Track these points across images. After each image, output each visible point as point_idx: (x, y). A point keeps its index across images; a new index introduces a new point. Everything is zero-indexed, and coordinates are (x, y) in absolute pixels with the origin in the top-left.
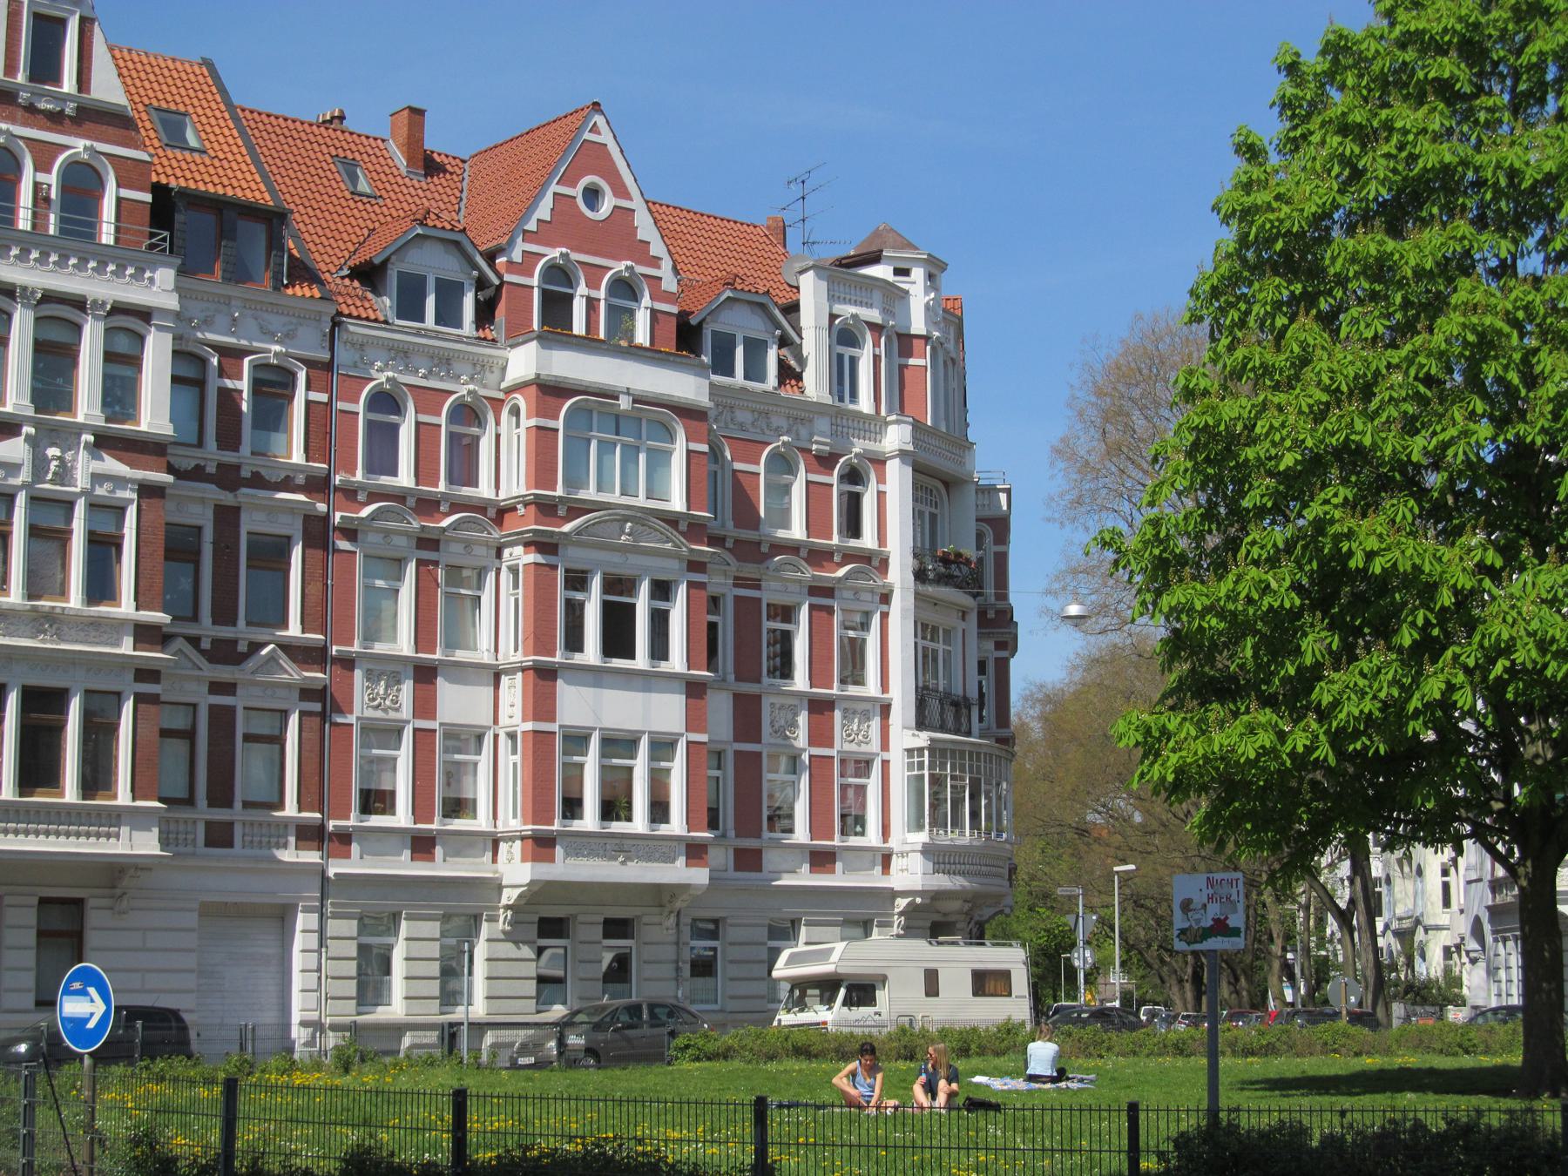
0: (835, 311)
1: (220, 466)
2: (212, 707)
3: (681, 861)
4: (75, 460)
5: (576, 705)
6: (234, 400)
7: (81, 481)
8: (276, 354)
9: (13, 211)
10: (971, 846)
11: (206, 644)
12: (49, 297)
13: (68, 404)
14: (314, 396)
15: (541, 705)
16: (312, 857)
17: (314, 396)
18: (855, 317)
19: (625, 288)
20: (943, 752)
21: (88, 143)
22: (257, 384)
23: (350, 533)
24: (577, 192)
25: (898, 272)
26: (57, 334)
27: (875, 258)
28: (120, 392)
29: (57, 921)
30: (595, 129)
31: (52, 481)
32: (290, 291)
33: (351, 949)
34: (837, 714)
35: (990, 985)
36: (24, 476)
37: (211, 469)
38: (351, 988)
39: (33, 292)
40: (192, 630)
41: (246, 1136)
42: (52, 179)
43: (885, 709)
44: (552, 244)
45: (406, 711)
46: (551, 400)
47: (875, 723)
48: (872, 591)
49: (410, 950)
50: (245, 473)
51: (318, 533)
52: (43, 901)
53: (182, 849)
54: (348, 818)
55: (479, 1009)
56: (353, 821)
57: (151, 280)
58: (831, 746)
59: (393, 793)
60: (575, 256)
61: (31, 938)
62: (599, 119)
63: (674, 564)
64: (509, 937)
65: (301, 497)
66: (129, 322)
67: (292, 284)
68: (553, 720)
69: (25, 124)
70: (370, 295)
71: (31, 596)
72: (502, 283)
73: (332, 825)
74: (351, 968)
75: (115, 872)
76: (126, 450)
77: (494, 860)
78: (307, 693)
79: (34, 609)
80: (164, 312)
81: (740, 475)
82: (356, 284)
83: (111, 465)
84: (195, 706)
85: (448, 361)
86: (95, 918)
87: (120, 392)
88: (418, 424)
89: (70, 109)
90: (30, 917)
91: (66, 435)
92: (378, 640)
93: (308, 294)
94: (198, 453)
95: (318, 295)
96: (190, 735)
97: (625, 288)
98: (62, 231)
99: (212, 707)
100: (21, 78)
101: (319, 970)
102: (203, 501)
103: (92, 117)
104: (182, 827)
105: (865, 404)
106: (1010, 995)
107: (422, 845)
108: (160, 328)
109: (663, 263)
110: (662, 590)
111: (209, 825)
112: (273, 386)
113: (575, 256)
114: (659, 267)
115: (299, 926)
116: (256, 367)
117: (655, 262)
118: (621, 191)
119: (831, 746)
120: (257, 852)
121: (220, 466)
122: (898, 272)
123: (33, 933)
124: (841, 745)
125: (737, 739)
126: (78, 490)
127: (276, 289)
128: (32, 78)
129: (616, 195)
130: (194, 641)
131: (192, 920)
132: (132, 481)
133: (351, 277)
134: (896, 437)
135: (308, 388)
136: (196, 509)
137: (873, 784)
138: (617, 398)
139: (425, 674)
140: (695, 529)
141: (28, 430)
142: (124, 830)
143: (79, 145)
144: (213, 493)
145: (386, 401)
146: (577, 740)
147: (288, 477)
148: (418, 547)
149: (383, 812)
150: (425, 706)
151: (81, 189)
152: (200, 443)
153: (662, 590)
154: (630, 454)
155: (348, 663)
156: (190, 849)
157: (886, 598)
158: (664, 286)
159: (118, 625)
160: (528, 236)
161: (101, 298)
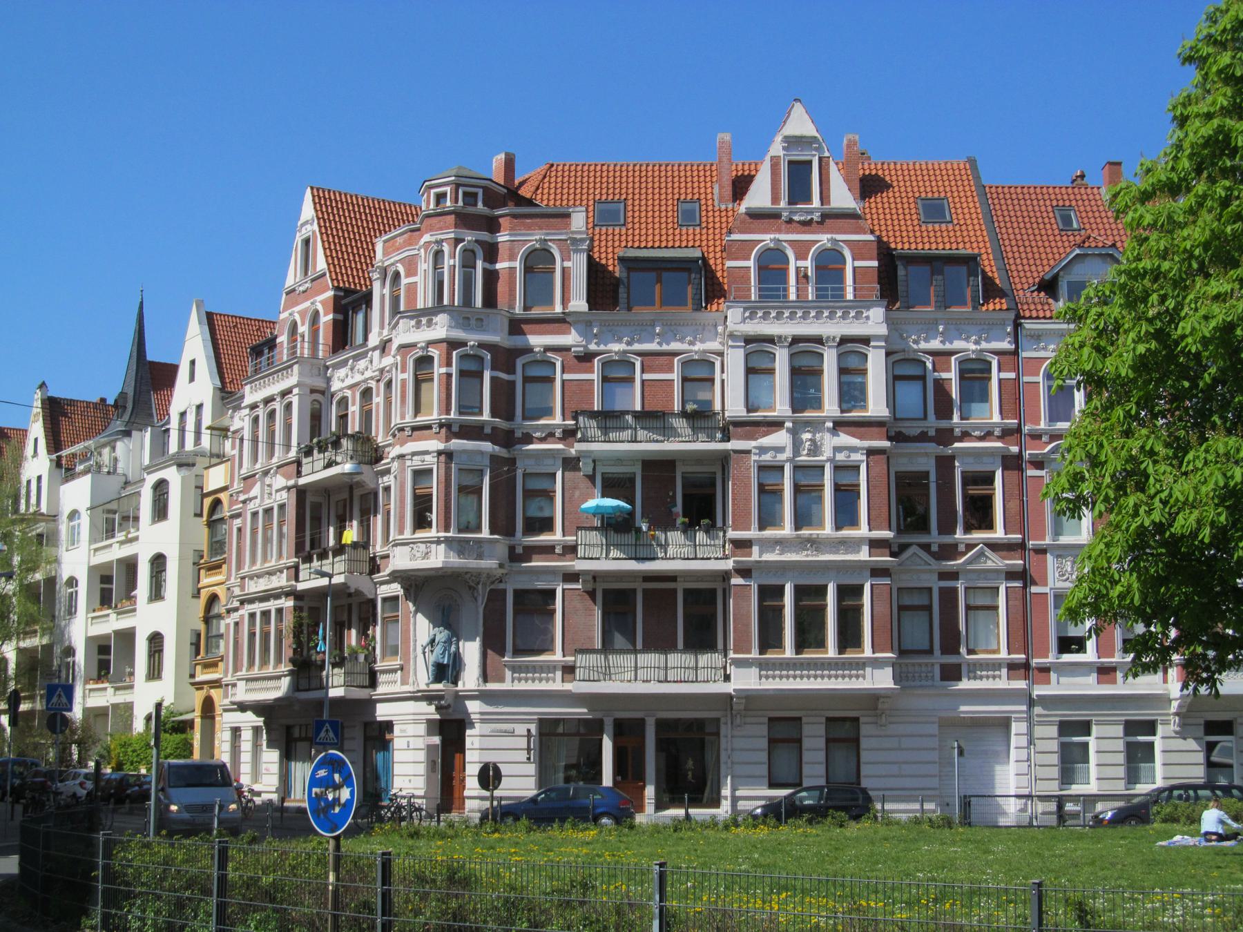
1: (938, 430)
2: (941, 589)
4: (822, 438)
6: (946, 387)
7: (827, 453)
8: (973, 352)
9: (843, 289)
10: (468, 715)
11: (935, 548)
12: (796, 340)
13: (818, 404)
14: (1004, 375)
16: (1021, 684)
17: (1004, 375)
21: (829, 236)
22: (963, 375)
23: (1038, 464)
26: (805, 362)
28: (852, 393)
29: (843, 731)
31: (808, 455)
32: (984, 308)
33: (1054, 746)
34: (1049, 557)
36: (788, 453)
37: (932, 433)
39: (786, 338)
40: (924, 539)
42: (808, 263)
49: (1104, 744)
51: (1013, 463)
52: (829, 720)
53: (907, 684)
54: (1047, 657)
55: (1092, 788)
56: (1051, 659)
57: (868, 318)
60: (783, 237)
61: (822, 743)
64: (1182, 735)
66: (852, 346)
67: (986, 301)
69: (787, 232)
70: (1051, 301)
71: (797, 528)
73: (1035, 661)
74: (1055, 759)
75: (873, 699)
76: (852, 429)
77: (1165, 681)
78: (1010, 575)
79: (798, 537)
80: (878, 338)
82: (1042, 294)
83: (845, 439)
84: (930, 589)
86: (865, 730)
87: (852, 393)
89: (816, 217)
90: (821, 730)
91: (815, 425)
93: (998, 307)
94: (921, 424)
95: (1005, 307)
96: (929, 608)
98: (760, 296)
99: (941, 589)
100: (783, 204)
101: (1029, 760)
102: (927, 454)
103: (831, 218)
104: (924, 669)
108: (829, 347)
111: (943, 666)
112: (975, 375)
113: (783, 237)
115: (1013, 731)
116: (961, 362)
120: (924, 683)
121: (938, 430)
123: (823, 740)
126: (824, 458)
127: (975, 308)
128: (790, 203)
130: (926, 547)
131: (934, 729)
132: (862, 449)
133: (1039, 290)
135: (1000, 370)
136: (923, 460)
141: (788, 424)
142: (868, 670)
143: (767, 239)
144: (933, 449)
149: (1078, 651)
151: (829, 267)
152: (925, 418)
155: (1042, 551)
156: (930, 683)
161: (832, 335)
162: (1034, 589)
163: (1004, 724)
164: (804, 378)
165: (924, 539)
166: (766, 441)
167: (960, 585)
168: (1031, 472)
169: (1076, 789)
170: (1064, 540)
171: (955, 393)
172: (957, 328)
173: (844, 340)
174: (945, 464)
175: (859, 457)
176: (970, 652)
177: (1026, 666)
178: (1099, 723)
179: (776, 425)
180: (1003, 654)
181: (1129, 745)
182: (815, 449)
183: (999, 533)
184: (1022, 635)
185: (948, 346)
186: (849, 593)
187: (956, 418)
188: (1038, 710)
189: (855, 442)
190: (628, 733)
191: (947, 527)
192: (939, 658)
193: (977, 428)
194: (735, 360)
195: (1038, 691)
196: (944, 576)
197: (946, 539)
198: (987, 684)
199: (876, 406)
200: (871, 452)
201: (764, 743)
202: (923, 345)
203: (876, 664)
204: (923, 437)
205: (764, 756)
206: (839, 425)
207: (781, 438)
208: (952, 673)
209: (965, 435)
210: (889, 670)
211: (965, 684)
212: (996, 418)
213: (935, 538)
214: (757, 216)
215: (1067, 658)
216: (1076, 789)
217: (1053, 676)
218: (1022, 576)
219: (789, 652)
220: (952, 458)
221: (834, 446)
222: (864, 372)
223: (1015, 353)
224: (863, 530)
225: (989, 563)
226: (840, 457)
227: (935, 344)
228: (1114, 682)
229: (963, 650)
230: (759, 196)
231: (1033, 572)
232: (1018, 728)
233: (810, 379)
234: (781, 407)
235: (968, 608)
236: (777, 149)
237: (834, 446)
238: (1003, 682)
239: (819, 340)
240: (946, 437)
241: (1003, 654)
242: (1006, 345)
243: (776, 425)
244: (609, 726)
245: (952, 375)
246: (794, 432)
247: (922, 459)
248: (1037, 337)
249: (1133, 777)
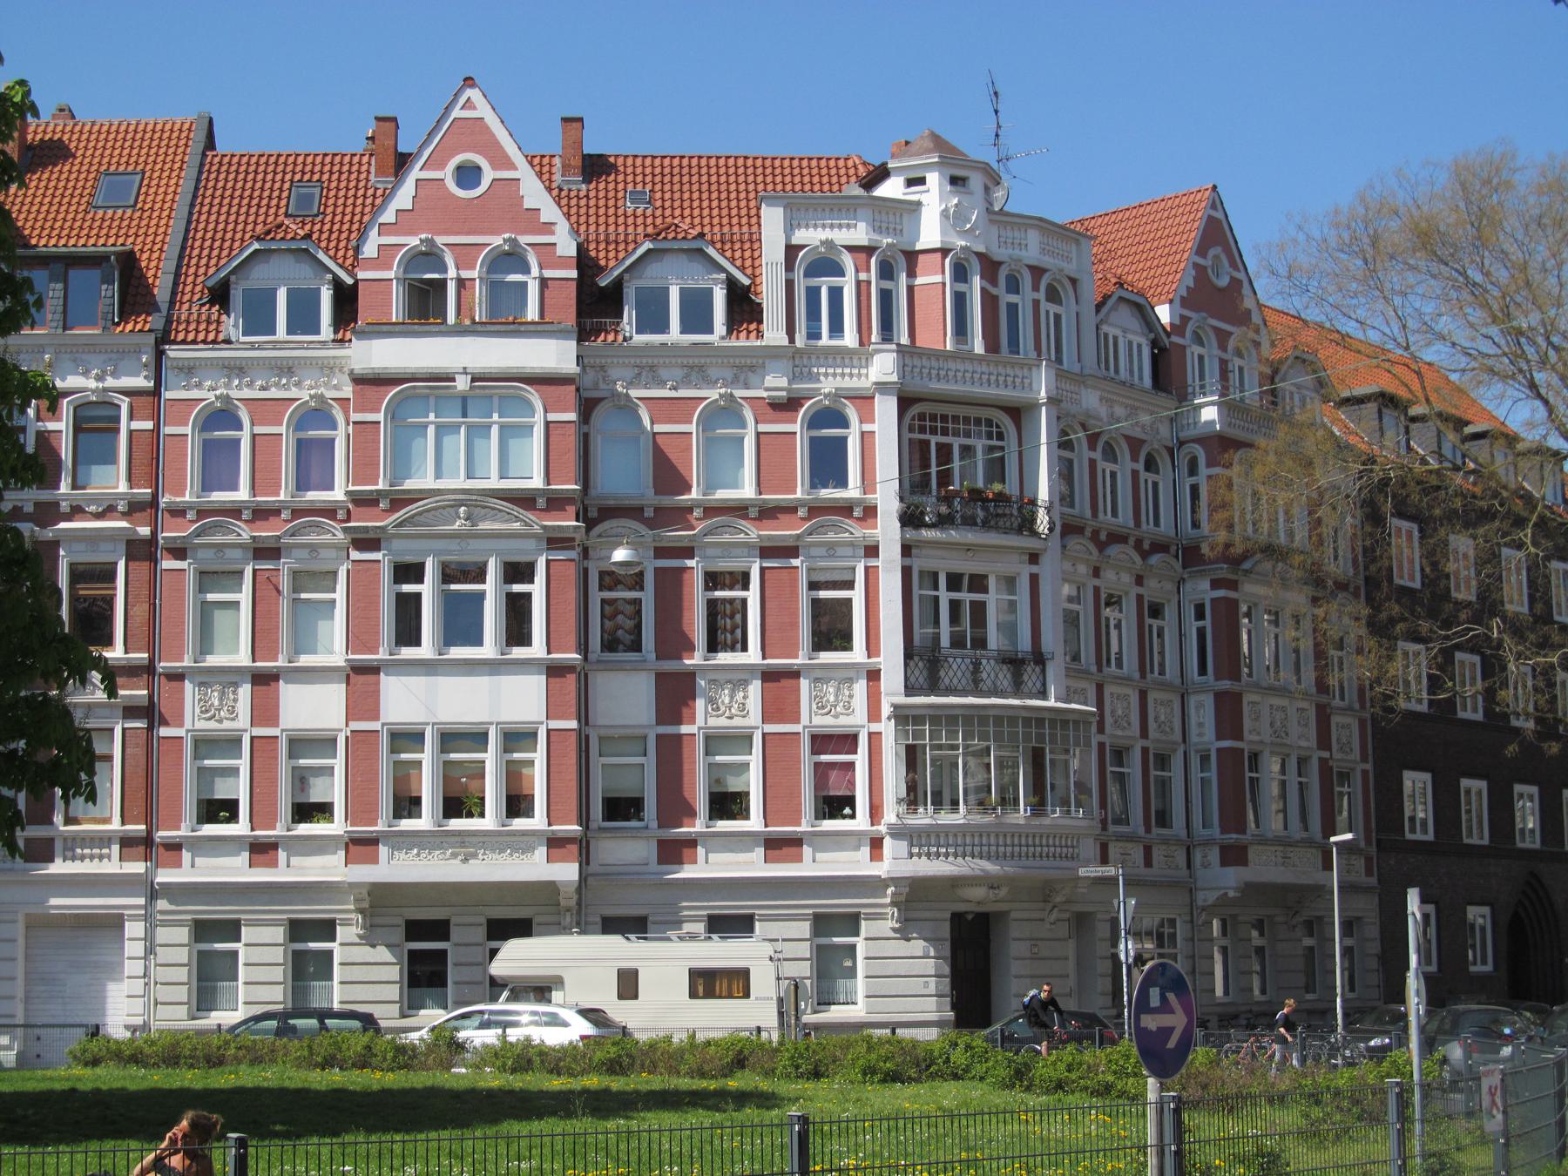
0: (795, 241)
1: (37, 504)
3: (542, 851)
5: (404, 700)
14: (136, 425)
15: (362, 703)
16: (138, 867)
17: (136, 425)
18: (829, 244)
19: (512, 258)
20: (918, 720)
25: (911, 182)
30: (469, 104)
33: (183, 955)
34: (804, 684)
35: (721, 985)
38: (182, 993)
43: (873, 675)
44: (411, 232)
45: (243, 719)
46: (371, 391)
47: (860, 687)
48: (852, 545)
50: (65, 506)
58: (797, 720)
59: (748, 794)
62: (473, 94)
63: (531, 544)
65: (124, 524)
68: (376, 717)
72: (357, 281)
81: (659, 440)
88: (758, 434)
92: (211, 653)
97: (512, 258)
105: (850, 339)
106: (747, 995)
107: (262, 850)
109: (558, 229)
110: (518, 571)
114: (552, 233)
117: (548, 228)
119: (797, 720)
121: (37, 504)
122: (911, 182)
124: (812, 718)
125: (659, 722)
129: (495, 167)
134: (883, 366)
135: (131, 417)
137: (860, 759)
138: (453, 380)
139: (264, 680)
140: (555, 502)
145: (223, 416)
146: (406, 738)
147: (15, 508)
148: (255, 558)
150: (265, 712)
153: (518, 571)
154: (478, 432)
155: (177, 677)
157: (872, 551)
158: (560, 251)
160: (384, 229)
228: (274, 864)
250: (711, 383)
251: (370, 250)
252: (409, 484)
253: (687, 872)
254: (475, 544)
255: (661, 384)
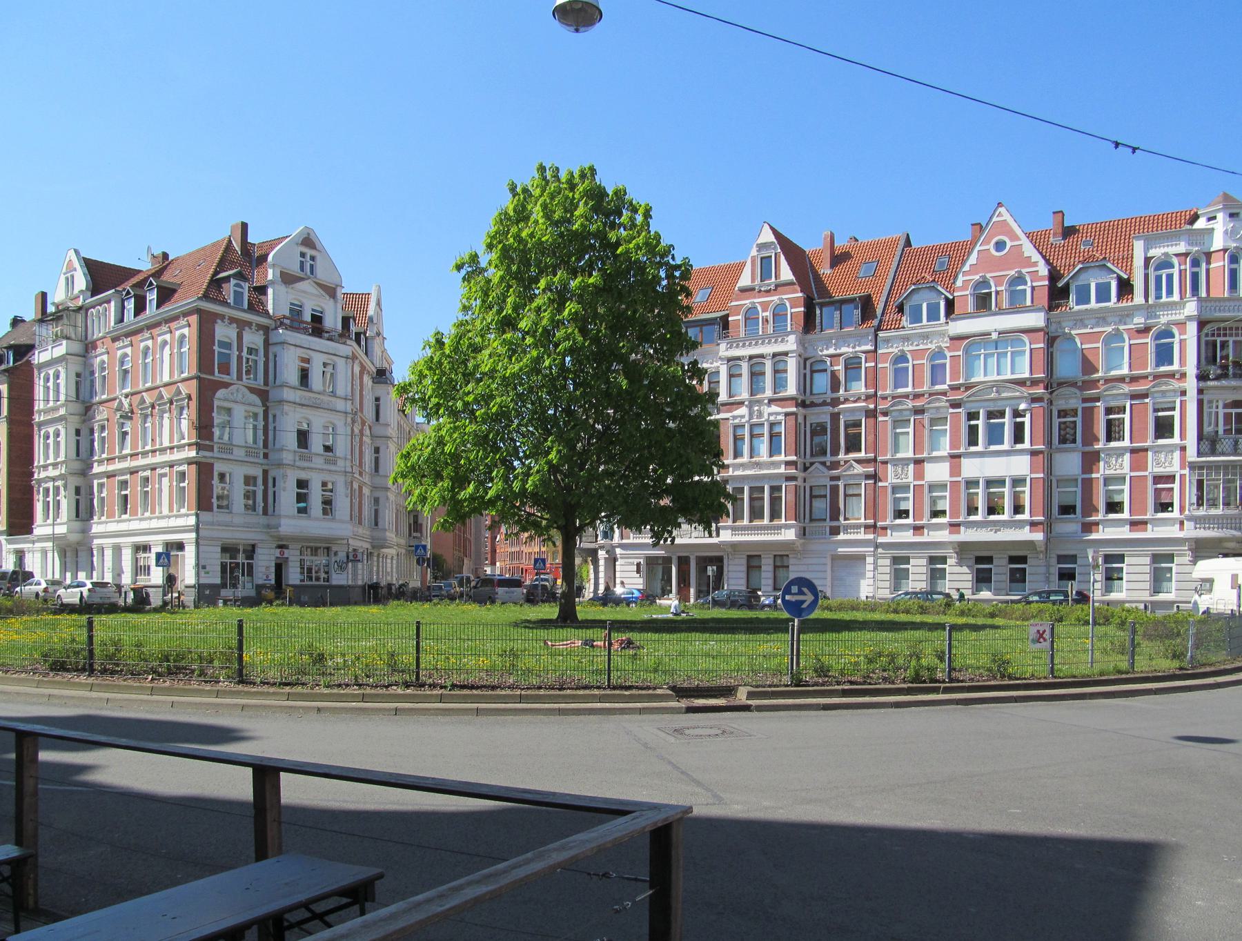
3: (1028, 528)
12: (751, 357)
16: (871, 536)
23: (885, 414)
24: (991, 247)
27: (1195, 218)
28: (779, 384)
33: (888, 570)
34: (1150, 454)
36: (747, 418)
41: (426, 660)
45: (911, 479)
56: (1100, 516)
62: (1001, 210)
64: (960, 564)
78: (868, 477)
80: (792, 352)
83: (774, 408)
85: (1104, 319)
89: (772, 287)
90: (771, 561)
91: (760, 402)
107: (955, 527)
111: (831, 528)
118: (1014, 237)
122: (1209, 219)
129: (1012, 240)
130: (823, 464)
139: (918, 462)
143: (747, 302)
150: (919, 475)
151: (779, 315)
155: (885, 463)
159: (779, 463)
162: (880, 484)
163: (862, 558)
164: (756, 375)
165: (822, 459)
166: (736, 413)
167: (841, 484)
168: (881, 419)
169: (1162, 597)
170: (899, 456)
171: (842, 378)
172: (842, 339)
173: (775, 355)
174: (835, 417)
175: (781, 417)
176: (846, 519)
177: (875, 526)
178: (1178, 555)
179: (741, 403)
180: (862, 520)
181: (932, 570)
182: (760, 415)
183: (862, 454)
184: (873, 509)
185: (838, 351)
186: (775, 489)
187: (842, 391)
188: (880, 550)
189: (778, 409)
190: (683, 562)
191: (835, 452)
192: (828, 523)
193: (853, 395)
194: (724, 371)
195: (881, 540)
196: (833, 478)
197: (834, 459)
198: (852, 536)
199: (791, 390)
200: (787, 414)
201: (744, 568)
202: (825, 352)
203: (787, 527)
204: (824, 404)
205: (744, 575)
206: (771, 401)
207: (743, 411)
208: (835, 531)
209: (846, 400)
210: (793, 530)
211: (842, 537)
212: (863, 390)
213: (829, 458)
214: (744, 290)
215: (1112, 516)
216: (1162, 597)
217: (1149, 526)
218: (874, 477)
219: (746, 522)
220: (839, 414)
221: (775, 412)
222: (786, 371)
223: (875, 351)
224: (782, 457)
225: (856, 471)
226: (772, 418)
227: (832, 351)
228: (1146, 530)
229: (841, 518)
230: (745, 280)
231: (880, 474)
232: (870, 560)
233: (761, 378)
234: (744, 395)
235: (846, 495)
236: (754, 252)
237: (775, 412)
238: (862, 535)
239: (762, 356)
240: (835, 402)
241: (862, 520)
242: (870, 347)
243: (741, 403)
244: (675, 561)
245: (840, 368)
246: (750, 407)
247: (822, 416)
248: (887, 340)
249: (896, 587)
250: (1109, 324)
251: (959, 283)
252: (973, 380)
253: (1094, 536)
254: (1000, 403)
255: (1086, 327)
